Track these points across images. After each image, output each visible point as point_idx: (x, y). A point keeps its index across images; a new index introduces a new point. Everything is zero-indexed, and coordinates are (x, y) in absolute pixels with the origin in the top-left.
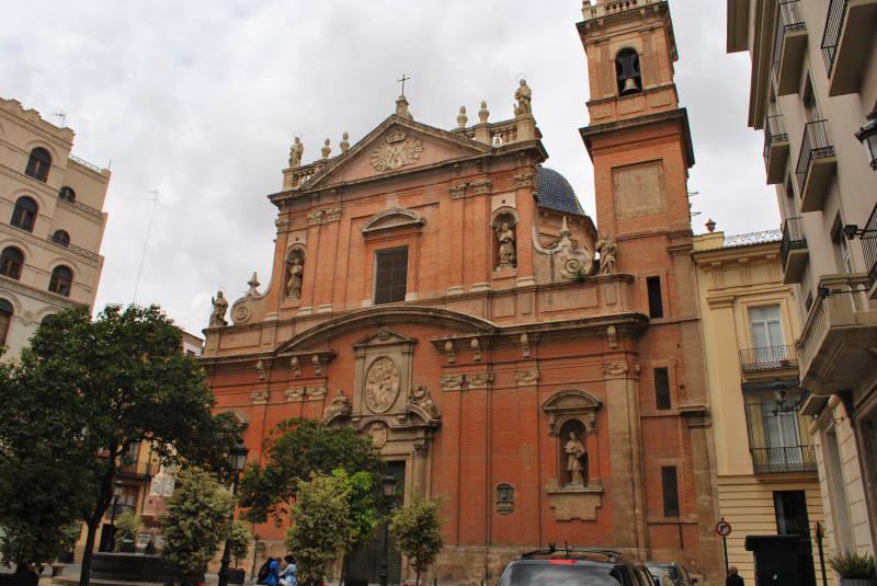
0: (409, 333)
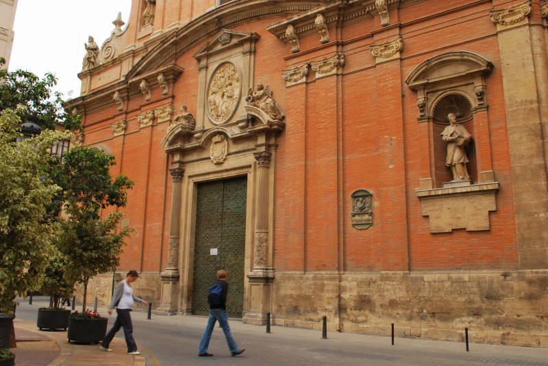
0: (246, 31)
